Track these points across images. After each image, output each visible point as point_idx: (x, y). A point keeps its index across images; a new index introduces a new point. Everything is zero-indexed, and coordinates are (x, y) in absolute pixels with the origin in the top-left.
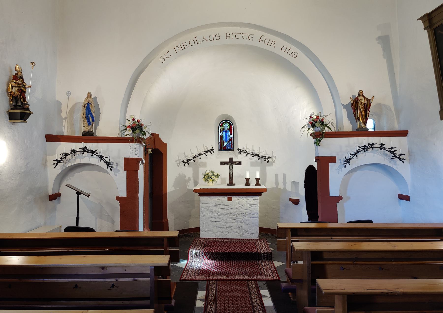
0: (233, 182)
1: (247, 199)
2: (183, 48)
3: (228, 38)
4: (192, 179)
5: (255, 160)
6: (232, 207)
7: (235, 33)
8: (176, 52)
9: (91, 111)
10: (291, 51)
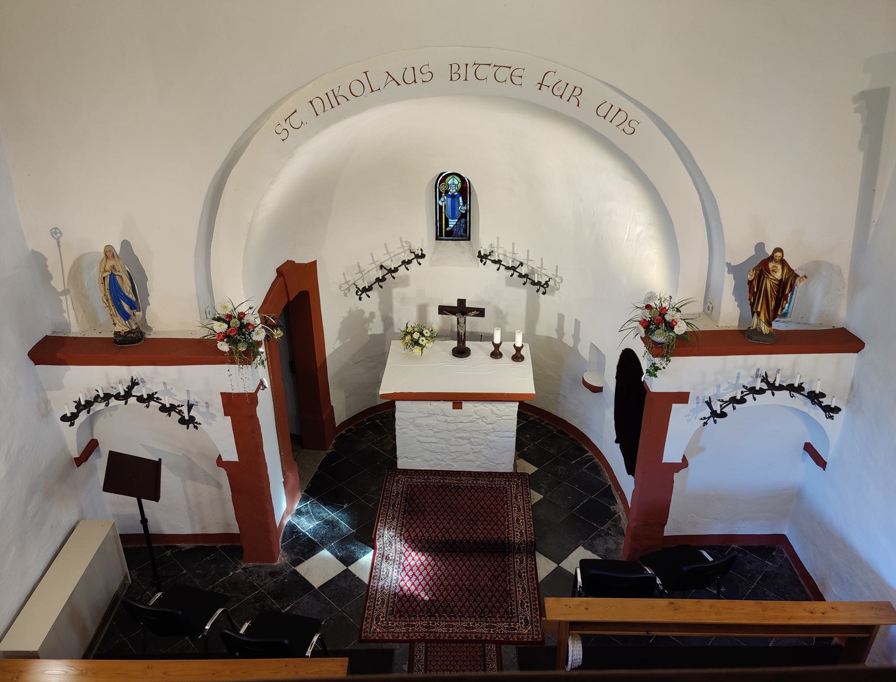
1: (493, 406)
2: (334, 103)
3: (455, 77)
4: (378, 314)
7: (475, 64)
8: (317, 115)
9: (122, 292)
10: (621, 117)
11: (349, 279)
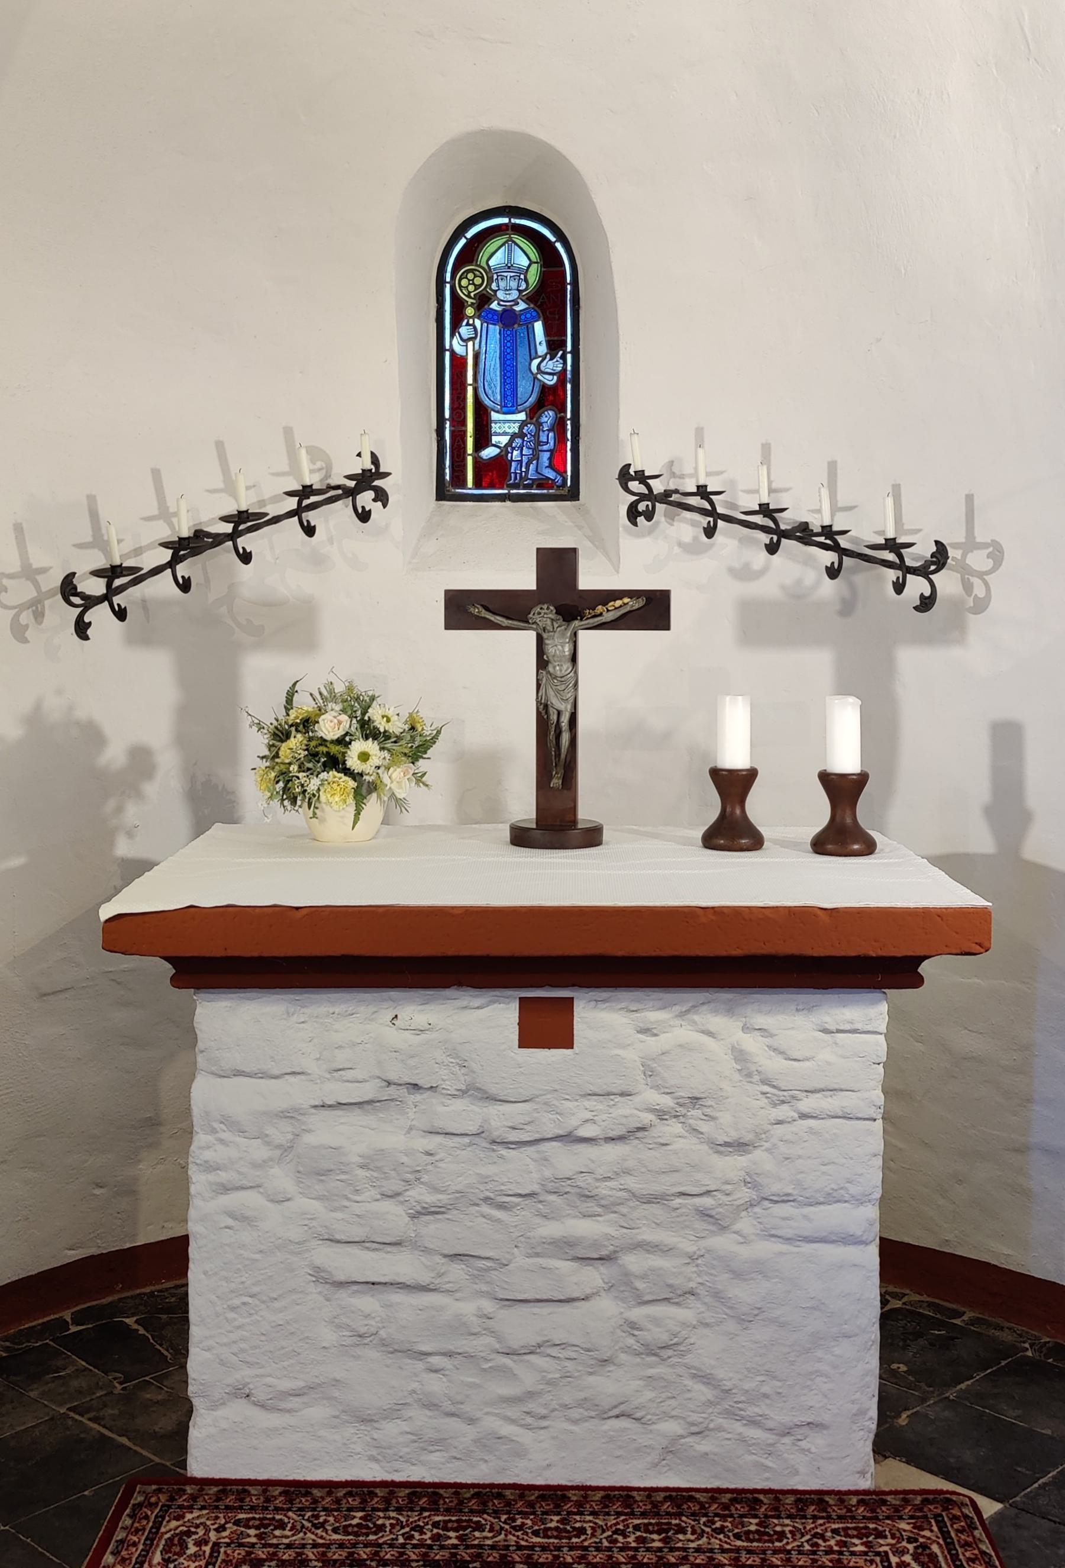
0: (574, 810)
1: (746, 1029)
5: (783, 587)
6: (574, 1122)
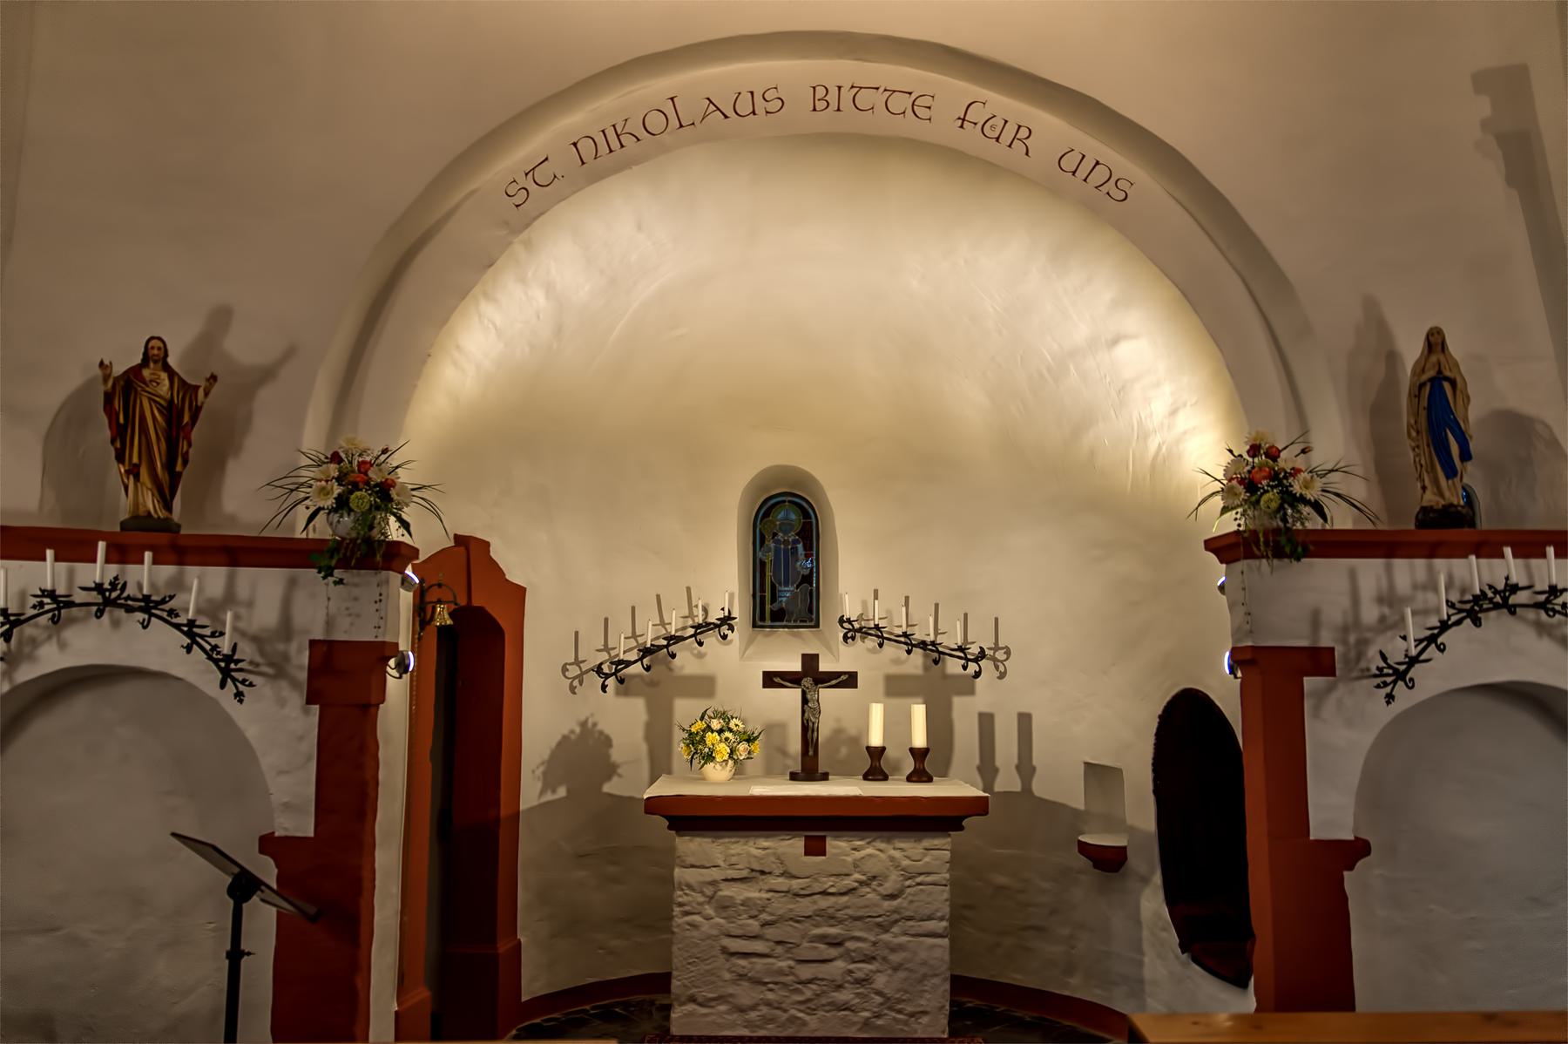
1: (894, 849)
2: (615, 144)
3: (820, 105)
6: (826, 886)
7: (852, 87)
8: (583, 163)
10: (1100, 175)
11: (584, 659)
